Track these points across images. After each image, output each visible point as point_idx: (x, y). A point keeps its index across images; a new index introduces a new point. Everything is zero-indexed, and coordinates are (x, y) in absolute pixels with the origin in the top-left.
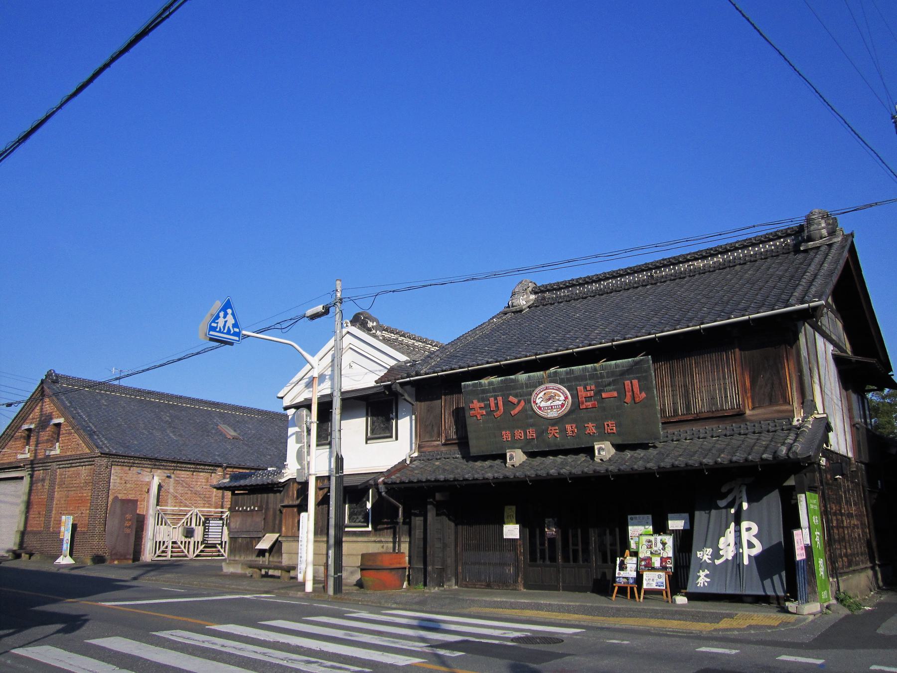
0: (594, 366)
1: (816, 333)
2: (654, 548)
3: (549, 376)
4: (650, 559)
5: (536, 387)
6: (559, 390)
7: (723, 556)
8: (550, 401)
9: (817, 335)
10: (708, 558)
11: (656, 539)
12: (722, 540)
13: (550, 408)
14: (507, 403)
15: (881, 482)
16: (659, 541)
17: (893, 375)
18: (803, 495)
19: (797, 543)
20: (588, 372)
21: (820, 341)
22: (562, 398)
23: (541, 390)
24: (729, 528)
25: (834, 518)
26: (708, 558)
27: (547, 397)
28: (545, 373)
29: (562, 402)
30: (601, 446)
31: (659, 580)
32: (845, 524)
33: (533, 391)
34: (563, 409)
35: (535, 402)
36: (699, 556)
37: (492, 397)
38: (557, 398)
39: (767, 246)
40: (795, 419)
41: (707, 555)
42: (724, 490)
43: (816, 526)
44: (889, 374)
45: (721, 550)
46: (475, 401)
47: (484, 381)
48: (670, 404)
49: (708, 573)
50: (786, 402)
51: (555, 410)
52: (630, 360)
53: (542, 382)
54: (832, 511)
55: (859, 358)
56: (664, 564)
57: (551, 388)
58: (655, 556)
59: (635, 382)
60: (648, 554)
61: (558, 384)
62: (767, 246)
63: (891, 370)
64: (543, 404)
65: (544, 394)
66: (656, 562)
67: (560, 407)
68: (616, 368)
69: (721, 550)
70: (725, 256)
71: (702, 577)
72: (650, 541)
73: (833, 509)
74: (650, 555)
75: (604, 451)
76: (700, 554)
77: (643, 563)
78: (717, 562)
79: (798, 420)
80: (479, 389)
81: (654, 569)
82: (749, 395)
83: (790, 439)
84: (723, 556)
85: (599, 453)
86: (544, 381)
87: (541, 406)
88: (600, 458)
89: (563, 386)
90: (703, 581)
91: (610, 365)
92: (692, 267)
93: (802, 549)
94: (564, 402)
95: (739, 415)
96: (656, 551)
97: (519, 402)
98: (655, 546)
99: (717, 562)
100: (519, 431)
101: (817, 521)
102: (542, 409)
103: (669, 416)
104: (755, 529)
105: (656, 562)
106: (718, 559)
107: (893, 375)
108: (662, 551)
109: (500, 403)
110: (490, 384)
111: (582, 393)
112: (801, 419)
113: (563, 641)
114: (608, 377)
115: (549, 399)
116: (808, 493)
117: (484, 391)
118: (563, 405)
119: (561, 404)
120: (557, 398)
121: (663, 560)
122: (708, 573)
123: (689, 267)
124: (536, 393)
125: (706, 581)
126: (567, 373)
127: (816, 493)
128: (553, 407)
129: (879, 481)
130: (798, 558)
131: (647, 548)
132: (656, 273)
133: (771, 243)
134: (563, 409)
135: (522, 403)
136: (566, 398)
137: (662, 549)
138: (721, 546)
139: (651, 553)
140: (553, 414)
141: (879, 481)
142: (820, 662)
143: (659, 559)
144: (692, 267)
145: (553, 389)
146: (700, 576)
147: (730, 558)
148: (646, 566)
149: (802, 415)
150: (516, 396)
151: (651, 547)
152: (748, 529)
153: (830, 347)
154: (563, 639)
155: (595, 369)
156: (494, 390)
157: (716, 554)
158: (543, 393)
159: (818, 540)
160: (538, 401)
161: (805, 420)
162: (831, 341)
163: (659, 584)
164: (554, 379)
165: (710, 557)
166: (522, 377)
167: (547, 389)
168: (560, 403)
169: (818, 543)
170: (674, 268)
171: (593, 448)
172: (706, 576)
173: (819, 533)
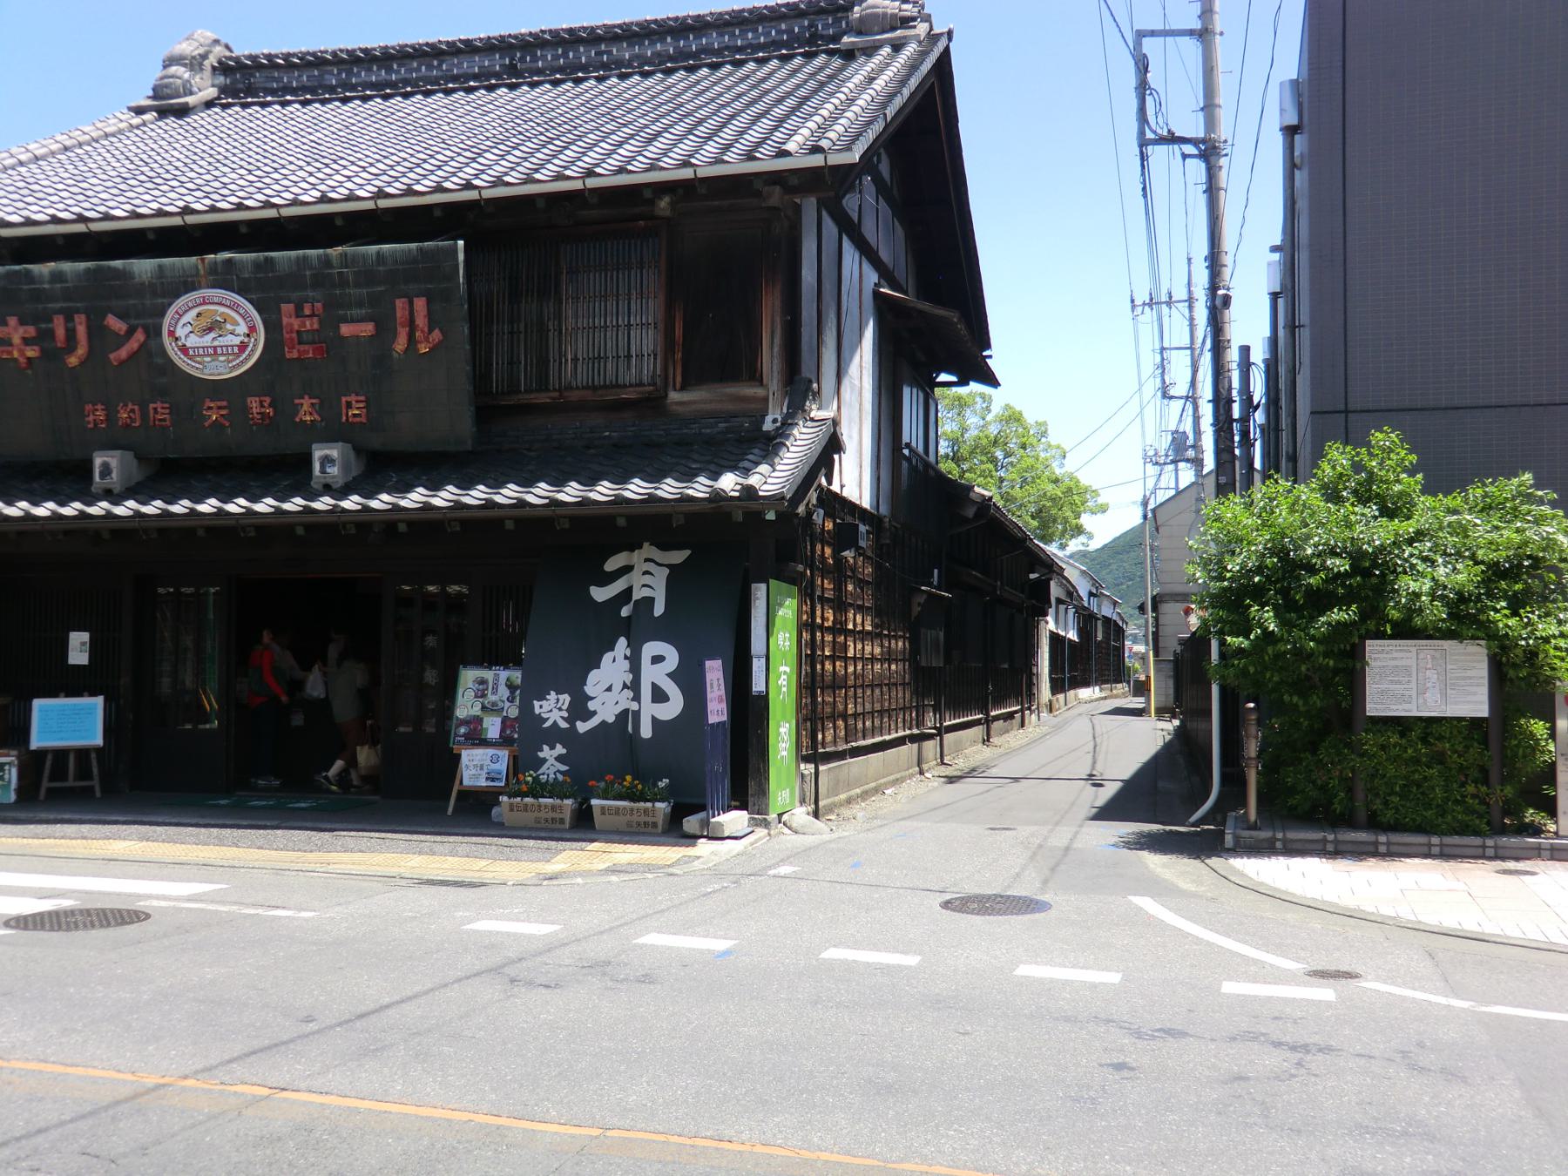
0: (327, 255)
1: (845, 238)
2: (492, 698)
3: (213, 269)
4: (479, 720)
5: (178, 296)
6: (234, 307)
7: (594, 713)
8: (212, 335)
9: (847, 245)
10: (562, 717)
11: (497, 677)
12: (593, 676)
13: (212, 352)
14: (97, 332)
15: (939, 573)
16: (503, 680)
17: (990, 357)
18: (763, 586)
19: (712, 685)
20: (311, 268)
21: (850, 254)
22: (242, 328)
23: (190, 305)
24: (613, 650)
25: (828, 638)
26: (562, 717)
27: (204, 322)
28: (203, 260)
29: (242, 338)
30: (327, 452)
31: (492, 765)
32: (851, 653)
33: (170, 305)
34: (244, 356)
35: (172, 333)
36: (537, 711)
37: (59, 312)
38: (229, 327)
39: (773, 33)
40: (769, 419)
41: (560, 709)
42: (611, 565)
43: (784, 654)
44: (984, 354)
45: (592, 698)
46: (13, 321)
47: (43, 269)
48: (503, 364)
49: (564, 751)
50: (756, 377)
51: (221, 358)
52: (413, 246)
53: (193, 282)
54: (826, 625)
55: (925, 306)
56: (508, 732)
57: (216, 300)
58: (491, 715)
59: (420, 304)
60: (476, 711)
61: (233, 291)
62: (773, 33)
63: (988, 346)
64: (193, 341)
65: (199, 315)
66: (492, 727)
67: (236, 350)
68: (378, 264)
69: (592, 698)
70: (682, 43)
71: (551, 761)
72: (483, 682)
73: (828, 620)
74: (479, 713)
75: (334, 466)
76: (541, 707)
77: (462, 730)
78: (582, 727)
79: (775, 421)
80: (25, 287)
81: (485, 743)
82: (679, 356)
83: (750, 461)
84: (594, 713)
85: (323, 471)
86: (200, 282)
87: (188, 345)
88: (323, 481)
89: (247, 299)
90: (553, 770)
91: (364, 256)
92: (605, 57)
93: (720, 701)
94: (246, 340)
95: (652, 403)
96: (494, 704)
97: (131, 332)
98: (493, 693)
99: (582, 727)
100: (130, 406)
101: (787, 643)
102: (191, 352)
103: (497, 391)
104: (672, 657)
105: (492, 727)
106: (584, 721)
107: (990, 357)
108: (507, 704)
109: (81, 330)
110: (57, 277)
111: (289, 320)
112: (780, 419)
113: (148, 916)
114: (357, 285)
115: (210, 329)
116: (772, 582)
117: (38, 296)
118: (242, 347)
119: (238, 343)
120: (229, 327)
121: (508, 723)
122: (564, 751)
123: (599, 58)
124: (177, 312)
125: (558, 771)
126: (257, 266)
127: (795, 585)
128: (219, 350)
129: (936, 571)
130: (713, 719)
131: (476, 697)
132: (522, 59)
133: (783, 26)
134: (244, 356)
135: (139, 336)
136: (252, 329)
137: (508, 699)
138: (589, 689)
139: (484, 708)
140: (219, 370)
141: (936, 571)
142: (721, 945)
143: (498, 720)
144: (605, 57)
145: (220, 304)
146: (544, 760)
147: (611, 719)
148: (467, 736)
149: (785, 410)
150: (122, 316)
151: (484, 696)
152: (657, 659)
153: (872, 277)
154: (150, 912)
155: (327, 262)
156: (67, 295)
157: (580, 709)
158: (194, 313)
159: (785, 683)
160: (180, 332)
161: (790, 421)
162: (877, 263)
163: (493, 775)
164: (224, 278)
165: (566, 715)
166: (143, 267)
167: (204, 303)
168: (237, 341)
169: (784, 689)
170: (565, 55)
171: (307, 460)
172: (559, 759)
173: (788, 669)
